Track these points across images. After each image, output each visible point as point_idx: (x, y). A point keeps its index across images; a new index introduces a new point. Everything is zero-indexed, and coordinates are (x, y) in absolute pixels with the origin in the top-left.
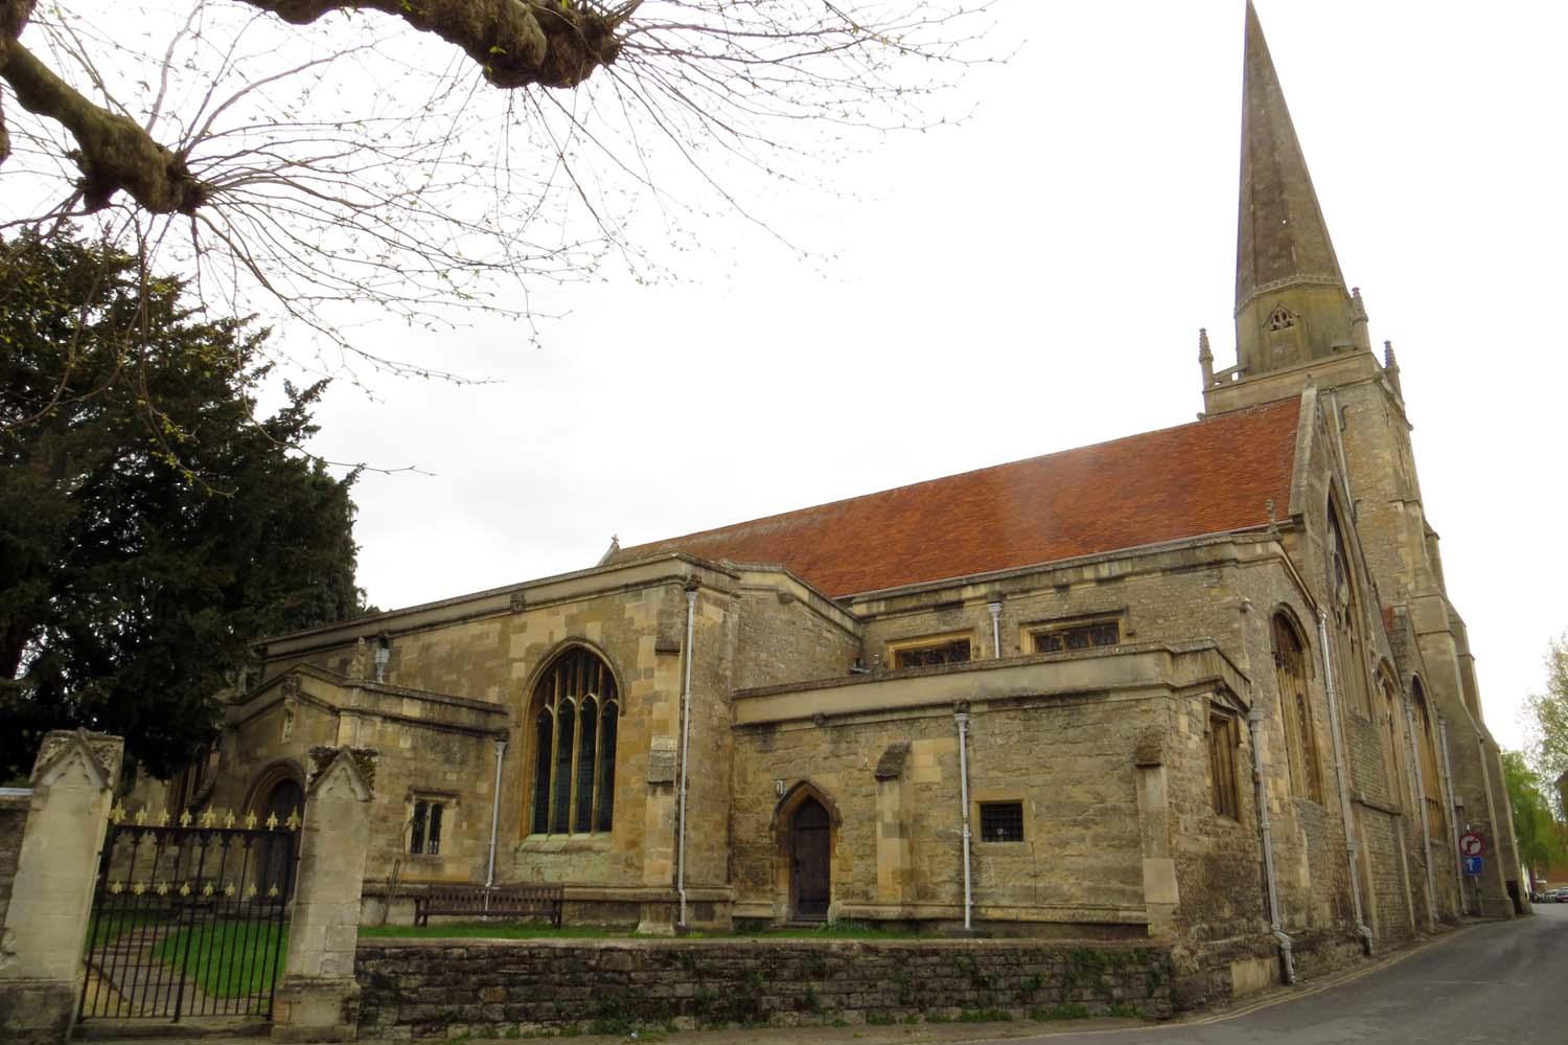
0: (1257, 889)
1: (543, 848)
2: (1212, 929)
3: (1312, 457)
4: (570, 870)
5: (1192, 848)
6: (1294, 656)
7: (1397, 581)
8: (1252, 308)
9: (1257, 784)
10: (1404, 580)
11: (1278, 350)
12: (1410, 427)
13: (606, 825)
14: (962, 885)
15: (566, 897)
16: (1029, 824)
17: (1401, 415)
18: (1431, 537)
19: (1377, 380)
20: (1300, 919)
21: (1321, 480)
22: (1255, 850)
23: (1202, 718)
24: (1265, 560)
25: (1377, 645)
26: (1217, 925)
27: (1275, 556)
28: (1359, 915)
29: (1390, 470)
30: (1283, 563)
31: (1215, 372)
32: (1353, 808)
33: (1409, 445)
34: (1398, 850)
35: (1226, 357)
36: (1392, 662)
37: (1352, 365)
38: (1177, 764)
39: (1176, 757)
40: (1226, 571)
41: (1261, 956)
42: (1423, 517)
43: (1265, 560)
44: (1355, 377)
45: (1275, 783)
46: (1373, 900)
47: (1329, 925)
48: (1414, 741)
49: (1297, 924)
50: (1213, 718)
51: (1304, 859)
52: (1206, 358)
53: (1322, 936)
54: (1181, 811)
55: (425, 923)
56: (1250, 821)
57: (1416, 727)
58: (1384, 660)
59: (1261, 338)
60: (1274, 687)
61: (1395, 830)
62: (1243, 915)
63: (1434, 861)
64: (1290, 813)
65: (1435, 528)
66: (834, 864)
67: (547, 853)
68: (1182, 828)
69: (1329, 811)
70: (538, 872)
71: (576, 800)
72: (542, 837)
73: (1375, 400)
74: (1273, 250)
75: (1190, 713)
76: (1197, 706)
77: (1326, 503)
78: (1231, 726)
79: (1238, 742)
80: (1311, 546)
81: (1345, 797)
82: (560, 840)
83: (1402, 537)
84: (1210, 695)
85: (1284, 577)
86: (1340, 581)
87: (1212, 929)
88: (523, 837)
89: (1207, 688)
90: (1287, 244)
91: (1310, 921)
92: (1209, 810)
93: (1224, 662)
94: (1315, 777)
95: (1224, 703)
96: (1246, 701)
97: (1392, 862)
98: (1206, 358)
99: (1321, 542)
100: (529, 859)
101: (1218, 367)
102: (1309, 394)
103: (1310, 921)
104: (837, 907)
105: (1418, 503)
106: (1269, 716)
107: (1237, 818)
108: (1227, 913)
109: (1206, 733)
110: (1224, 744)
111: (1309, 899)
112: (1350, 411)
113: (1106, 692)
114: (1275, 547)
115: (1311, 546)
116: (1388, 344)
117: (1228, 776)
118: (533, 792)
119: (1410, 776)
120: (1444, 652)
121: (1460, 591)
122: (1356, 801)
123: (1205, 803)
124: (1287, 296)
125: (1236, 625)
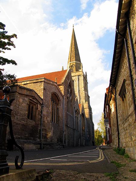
5: (19, 122)
34: (74, 134)
45: (47, 118)
50: (30, 102)
79: (37, 109)
96: (42, 103)
123: (25, 116)
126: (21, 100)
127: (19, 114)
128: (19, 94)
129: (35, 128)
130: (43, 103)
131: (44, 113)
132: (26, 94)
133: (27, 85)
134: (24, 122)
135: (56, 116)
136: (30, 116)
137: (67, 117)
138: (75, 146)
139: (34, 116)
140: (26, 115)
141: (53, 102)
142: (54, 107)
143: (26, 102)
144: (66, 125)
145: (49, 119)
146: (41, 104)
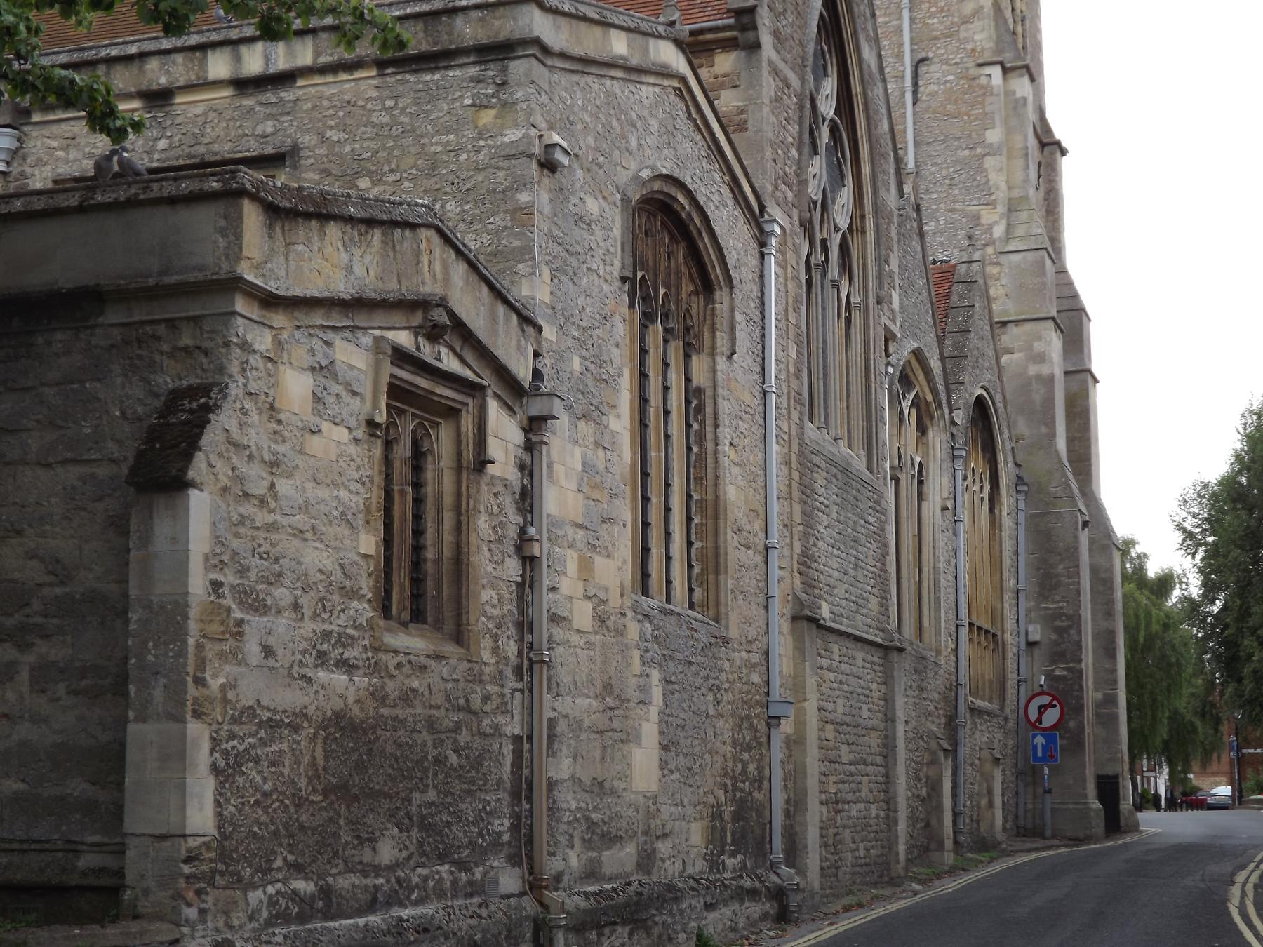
2: (326, 892)
5: (288, 698)
6: (696, 305)
7: (976, 218)
9: (529, 562)
10: (987, 217)
12: (1096, 381)
18: (1050, 147)
22: (504, 709)
23: (367, 389)
24: (635, 72)
25: (903, 310)
26: (344, 883)
27: (664, 72)
28: (778, 843)
30: (683, 91)
34: (889, 718)
38: (259, 488)
40: (518, 68)
43: (635, 72)
45: (586, 567)
46: (814, 814)
47: (697, 867)
48: (964, 515)
49: (607, 870)
50: (397, 392)
51: (650, 731)
53: (670, 894)
54: (260, 608)
58: (918, 354)
60: (620, 357)
61: (887, 680)
62: (442, 858)
63: (978, 738)
64: (621, 632)
65: (1059, 134)
68: (252, 649)
69: (733, 633)
75: (325, 370)
76: (353, 356)
78: (467, 422)
79: (482, 463)
80: (769, 86)
81: (780, 610)
83: (994, 136)
84: (404, 338)
86: (837, 179)
87: (326, 892)
89: (398, 318)
91: (646, 861)
92: (365, 611)
94: (708, 565)
95: (450, 364)
96: (522, 371)
97: (874, 741)
103: (646, 861)
105: (1032, 73)
106: (593, 414)
107: (459, 637)
108: (387, 852)
109: (371, 423)
117: (448, 538)
119: (945, 581)
120: (1041, 358)
123: (352, 594)
125: (524, 197)
126: (296, 387)
127: (282, 594)
128: (270, 301)
129: (464, 737)
130: (537, 375)
131: (560, 498)
132: (342, 288)
133: (287, 95)
134: (340, 678)
135: (677, 501)
136: (402, 579)
137: (807, 490)
138: (900, 869)
139: (446, 567)
140: (366, 586)
141: (647, 318)
142: (655, 383)
143: (355, 403)
144: (795, 618)
145: (615, 570)
146: (514, 390)
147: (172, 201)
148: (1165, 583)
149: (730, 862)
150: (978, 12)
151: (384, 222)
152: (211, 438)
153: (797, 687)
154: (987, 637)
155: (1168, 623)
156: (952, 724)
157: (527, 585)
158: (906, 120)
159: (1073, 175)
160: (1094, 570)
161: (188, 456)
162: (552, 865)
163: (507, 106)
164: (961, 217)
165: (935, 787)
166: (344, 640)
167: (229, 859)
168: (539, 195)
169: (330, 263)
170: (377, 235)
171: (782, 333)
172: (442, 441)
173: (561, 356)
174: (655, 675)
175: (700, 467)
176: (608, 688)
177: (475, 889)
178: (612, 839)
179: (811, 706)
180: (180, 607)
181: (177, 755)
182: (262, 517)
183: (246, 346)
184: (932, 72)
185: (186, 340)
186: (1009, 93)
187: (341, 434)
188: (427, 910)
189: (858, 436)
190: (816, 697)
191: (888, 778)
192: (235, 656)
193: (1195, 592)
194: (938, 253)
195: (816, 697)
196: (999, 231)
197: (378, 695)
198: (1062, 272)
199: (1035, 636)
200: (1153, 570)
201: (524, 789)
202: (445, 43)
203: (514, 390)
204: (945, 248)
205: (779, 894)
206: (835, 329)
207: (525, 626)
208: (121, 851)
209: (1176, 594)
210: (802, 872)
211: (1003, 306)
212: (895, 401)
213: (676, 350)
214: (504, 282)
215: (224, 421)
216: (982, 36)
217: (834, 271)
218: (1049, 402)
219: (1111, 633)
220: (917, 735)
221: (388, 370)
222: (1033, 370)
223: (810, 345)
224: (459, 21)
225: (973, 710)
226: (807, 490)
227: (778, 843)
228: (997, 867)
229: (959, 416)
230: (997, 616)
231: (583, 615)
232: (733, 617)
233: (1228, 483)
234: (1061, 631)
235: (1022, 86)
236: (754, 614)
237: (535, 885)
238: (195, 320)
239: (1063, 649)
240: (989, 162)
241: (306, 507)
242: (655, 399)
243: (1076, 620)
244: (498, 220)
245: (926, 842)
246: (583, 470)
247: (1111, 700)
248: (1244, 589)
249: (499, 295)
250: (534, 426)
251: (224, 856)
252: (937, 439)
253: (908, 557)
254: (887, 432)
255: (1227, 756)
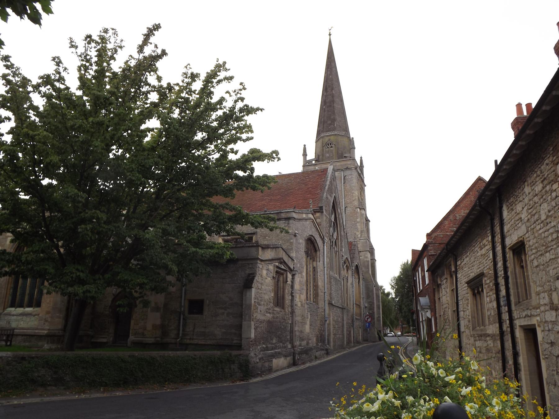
0: (288, 333)
1: (12, 313)
2: (267, 347)
3: (329, 188)
4: (22, 323)
5: (262, 318)
6: (314, 254)
7: (355, 234)
8: (321, 140)
9: (293, 296)
10: (357, 233)
11: (328, 155)
12: (365, 186)
13: (38, 305)
14: (179, 330)
15: (15, 333)
16: (206, 308)
17: (363, 181)
18: (367, 221)
19: (356, 168)
20: (304, 343)
21: (331, 196)
22: (289, 319)
23: (273, 272)
24: (306, 220)
25: (345, 253)
26: (269, 346)
27: (310, 219)
28: (326, 341)
29: (357, 198)
30: (313, 222)
31: (307, 159)
32: (329, 306)
33: (364, 191)
34: (343, 320)
35: (311, 155)
36: (349, 259)
37: (349, 162)
38: (260, 288)
39: (259, 285)
40: (291, 221)
41: (286, 356)
42: (366, 215)
43: (306, 220)
44: (349, 166)
45: (300, 296)
46: (332, 336)
47: (315, 345)
48: (354, 285)
49: (303, 345)
50: (277, 272)
51: (308, 323)
52: (305, 155)
53: (311, 349)
54: (260, 305)
55: (10, 345)
56: (288, 310)
57: (355, 281)
58: (347, 258)
59: (323, 150)
60: (304, 264)
61: (343, 314)
62: (281, 342)
63: (357, 323)
64: (304, 307)
65: (369, 219)
66: (132, 322)
67: (13, 315)
68: (259, 311)
69: (320, 306)
70: (9, 323)
71: (29, 294)
72: (13, 309)
73: (355, 174)
74: (329, 122)
75: (268, 270)
76: (271, 267)
77: (332, 204)
78: (285, 276)
79: (287, 281)
80: (325, 218)
81: (327, 302)
82: (20, 310)
83: (358, 220)
84: (277, 264)
85: (313, 226)
86: (334, 231)
87: (267, 347)
88: (4, 309)
89: (276, 261)
90: (334, 120)
91: (308, 343)
92: (272, 305)
93: (284, 253)
94: (316, 295)
95: (283, 267)
96: (292, 268)
97: (341, 324)
98: (305, 155)
99: (328, 217)
100: (6, 318)
101: (308, 158)
102: (330, 168)
103: (308, 343)
104: (132, 338)
105: (365, 209)
106: (301, 273)
107: (283, 308)
108: (274, 341)
109: (273, 277)
110: (282, 282)
111: (308, 336)
112: (347, 177)
113: (238, 260)
114: (311, 216)
115: (325, 218)
116: (361, 158)
117: (282, 293)
118: (11, 291)
119: (351, 296)
120: (367, 257)
121: (374, 240)
122: (330, 304)
123: (270, 302)
124: (332, 138)
125: (292, 241)
126: (265, 272)
128: (262, 261)
131: (297, 286)
132: (270, 258)
141: (308, 257)
142: (309, 267)
144: (329, 304)
145: (303, 297)
147: (249, 247)
148: (389, 294)
149: (320, 344)
150: (355, 199)
151: (275, 247)
152: (255, 281)
153: (329, 315)
154: (358, 306)
155: (389, 301)
156: (353, 321)
157: (292, 300)
158: (344, 218)
159: (372, 225)
160: (376, 294)
161: (252, 284)
162: (295, 344)
163: (289, 227)
164: (353, 233)
165: (350, 332)
166: (269, 309)
167: (256, 341)
168: (294, 240)
169: (269, 254)
170: (274, 250)
171: (327, 257)
172: (281, 279)
173: (297, 264)
174: (309, 313)
175: (315, 280)
176: (303, 316)
177: (285, 347)
178: (303, 340)
179: (331, 318)
180: (251, 305)
181: (250, 326)
182: (260, 292)
183: (259, 267)
184: (348, 209)
185: (250, 266)
186: (361, 213)
187: (270, 279)
188: (279, 350)
189: (338, 273)
190: (333, 316)
191: (343, 331)
192: (257, 312)
193: (394, 297)
194: (349, 240)
195: (333, 316)
196: (359, 236)
197: (273, 317)
198: (370, 242)
199: (366, 306)
200: (386, 292)
201: (292, 331)
202: (280, 217)
203: (291, 270)
204: (350, 240)
205: (327, 350)
206: (334, 254)
207: (292, 306)
208: (241, 340)
209: (390, 297)
210: (330, 346)
211: (360, 248)
212: (343, 266)
213: (311, 261)
214: (289, 253)
215: (256, 278)
216: (356, 203)
217: (334, 246)
218: (368, 265)
219: (379, 305)
220: (347, 323)
221: (276, 269)
222: (365, 259)
223: (331, 259)
224: (282, 214)
225: (356, 319)
226: (330, 282)
227: (326, 341)
228: (360, 346)
229: (353, 268)
230: (360, 302)
231: (299, 304)
232: (320, 304)
233: (399, 277)
234: (371, 305)
235: (363, 212)
236: (323, 304)
237: (293, 347)
238: (252, 264)
239: (371, 308)
240: (358, 224)
241: (265, 290)
242: (308, 269)
243: (373, 303)
244: (288, 244)
245: (349, 342)
246: (300, 281)
247: (379, 317)
248: (402, 296)
249: (289, 256)
250: (293, 275)
251: (255, 341)
252: (350, 272)
253: (345, 292)
254: (342, 272)
255: (400, 327)
